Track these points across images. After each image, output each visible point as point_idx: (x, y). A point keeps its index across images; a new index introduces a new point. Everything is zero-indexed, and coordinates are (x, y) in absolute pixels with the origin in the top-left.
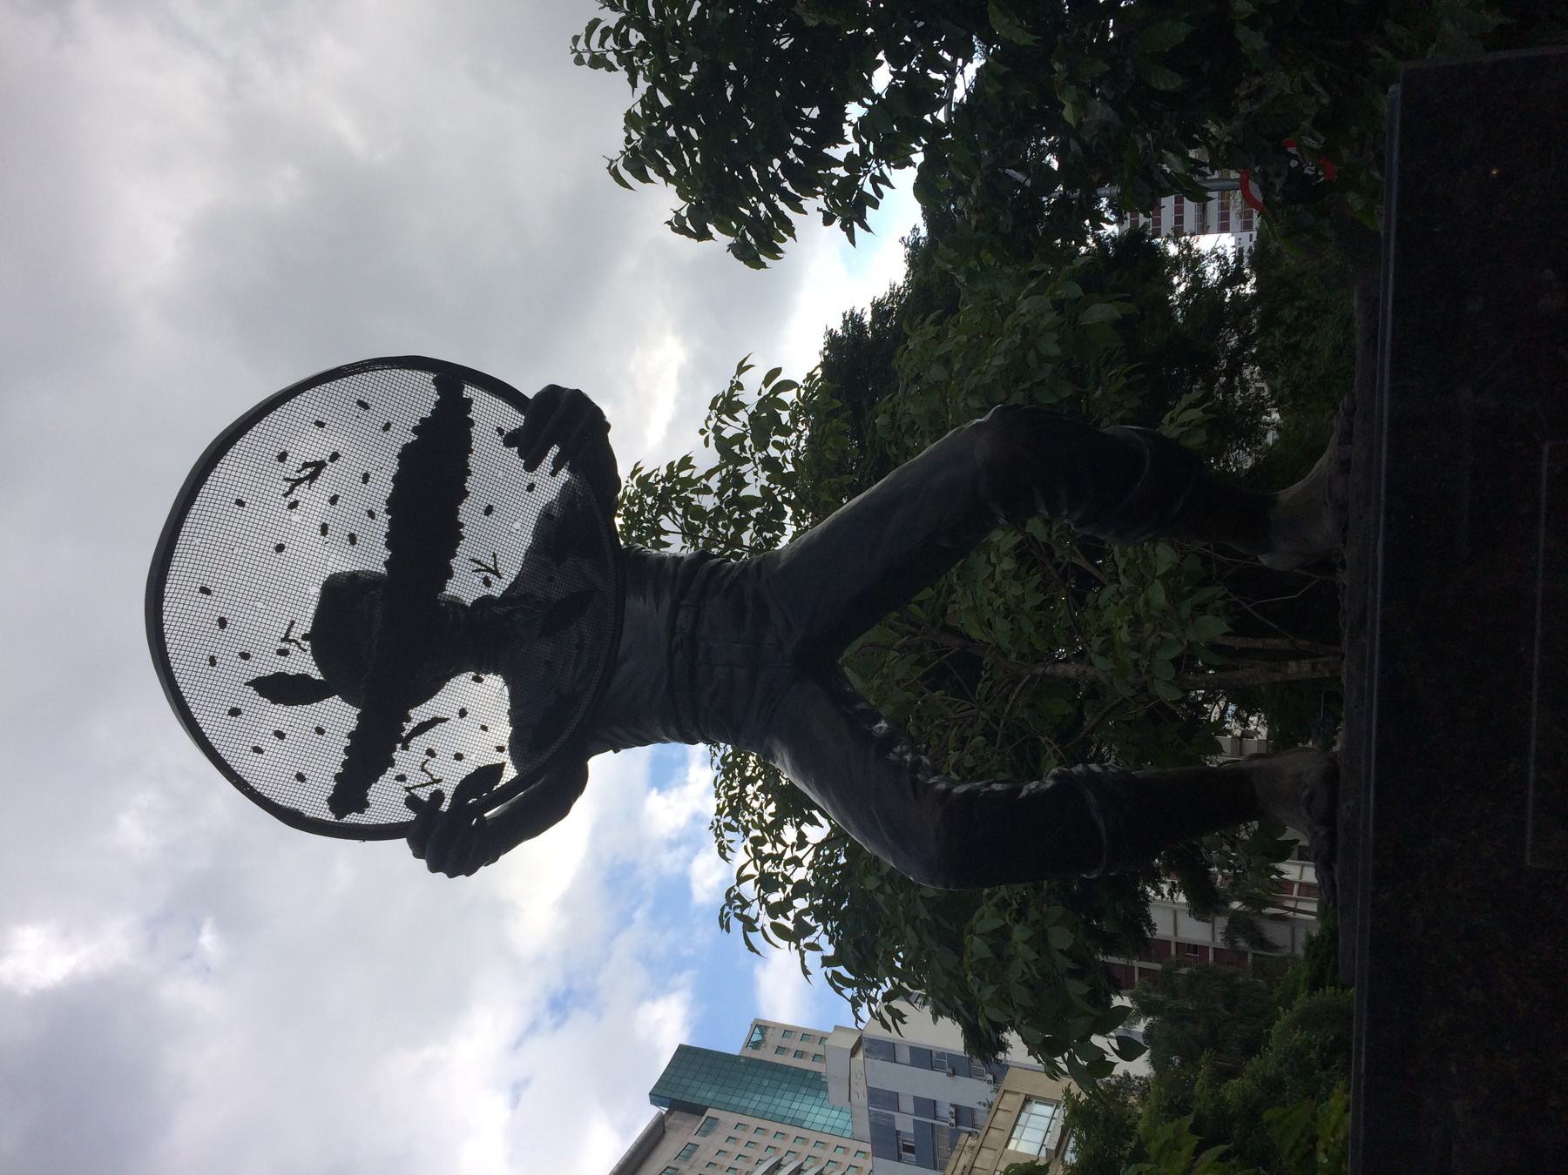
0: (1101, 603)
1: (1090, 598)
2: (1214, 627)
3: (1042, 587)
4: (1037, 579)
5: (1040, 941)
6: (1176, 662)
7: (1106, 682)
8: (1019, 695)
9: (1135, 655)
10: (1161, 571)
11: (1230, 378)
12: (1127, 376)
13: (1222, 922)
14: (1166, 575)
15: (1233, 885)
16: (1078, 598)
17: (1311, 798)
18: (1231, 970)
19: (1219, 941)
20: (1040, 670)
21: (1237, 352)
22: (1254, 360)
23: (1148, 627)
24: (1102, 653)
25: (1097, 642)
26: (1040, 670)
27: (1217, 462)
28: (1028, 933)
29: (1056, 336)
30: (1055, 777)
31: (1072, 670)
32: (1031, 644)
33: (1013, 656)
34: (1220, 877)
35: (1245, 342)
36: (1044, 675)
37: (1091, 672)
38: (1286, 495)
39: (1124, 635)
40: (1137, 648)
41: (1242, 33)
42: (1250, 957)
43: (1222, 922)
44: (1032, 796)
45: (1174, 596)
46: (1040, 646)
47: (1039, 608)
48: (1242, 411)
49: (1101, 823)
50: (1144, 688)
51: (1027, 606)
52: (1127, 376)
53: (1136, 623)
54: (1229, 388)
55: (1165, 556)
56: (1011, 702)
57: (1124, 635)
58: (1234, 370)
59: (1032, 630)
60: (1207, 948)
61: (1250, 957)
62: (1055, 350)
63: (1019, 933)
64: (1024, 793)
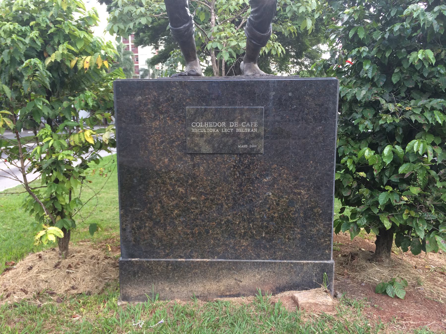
0: (232, 28)
1: (233, 25)
2: (226, 57)
3: (235, 11)
4: (237, 9)
5: (142, 15)
6: (217, 48)
7: (211, 30)
8: (205, 5)
9: (218, 37)
10: (240, 44)
11: (296, 63)
12: (294, 32)
13: (146, 67)
14: (238, 45)
15: (156, 70)
16: (233, 22)
17: (193, 71)
18: (134, 70)
19: (140, 67)
20: (213, 11)
21: (303, 64)
22: (301, 69)
23: (225, 41)
24: (218, 29)
25: (221, 27)
26: (213, 11)
27: (273, 61)
28: (143, 12)
29: (304, 11)
30: (191, 16)
31: (213, 20)
32: (219, 8)
33: (216, 3)
34: (159, 66)
35: (306, 67)
36: (211, 12)
37: (213, 26)
38: (256, 66)
39: (223, 34)
40: (220, 38)
41: (357, 49)
42: (138, 75)
43: (146, 67)
44: (186, 10)
45: (234, 48)
46: (219, 11)
47: (230, 10)
48: (286, 66)
49: (182, 27)
50: (209, 40)
51: (230, 7)
52: (294, 32)
53: (226, 37)
54: (293, 63)
55: (243, 45)
56: (203, 3)
57: (223, 34)
58: (298, 63)
59: (224, 9)
60: (138, 63)
61: (138, 75)
62: (300, 11)
63: (143, 9)
64: (187, 8)
